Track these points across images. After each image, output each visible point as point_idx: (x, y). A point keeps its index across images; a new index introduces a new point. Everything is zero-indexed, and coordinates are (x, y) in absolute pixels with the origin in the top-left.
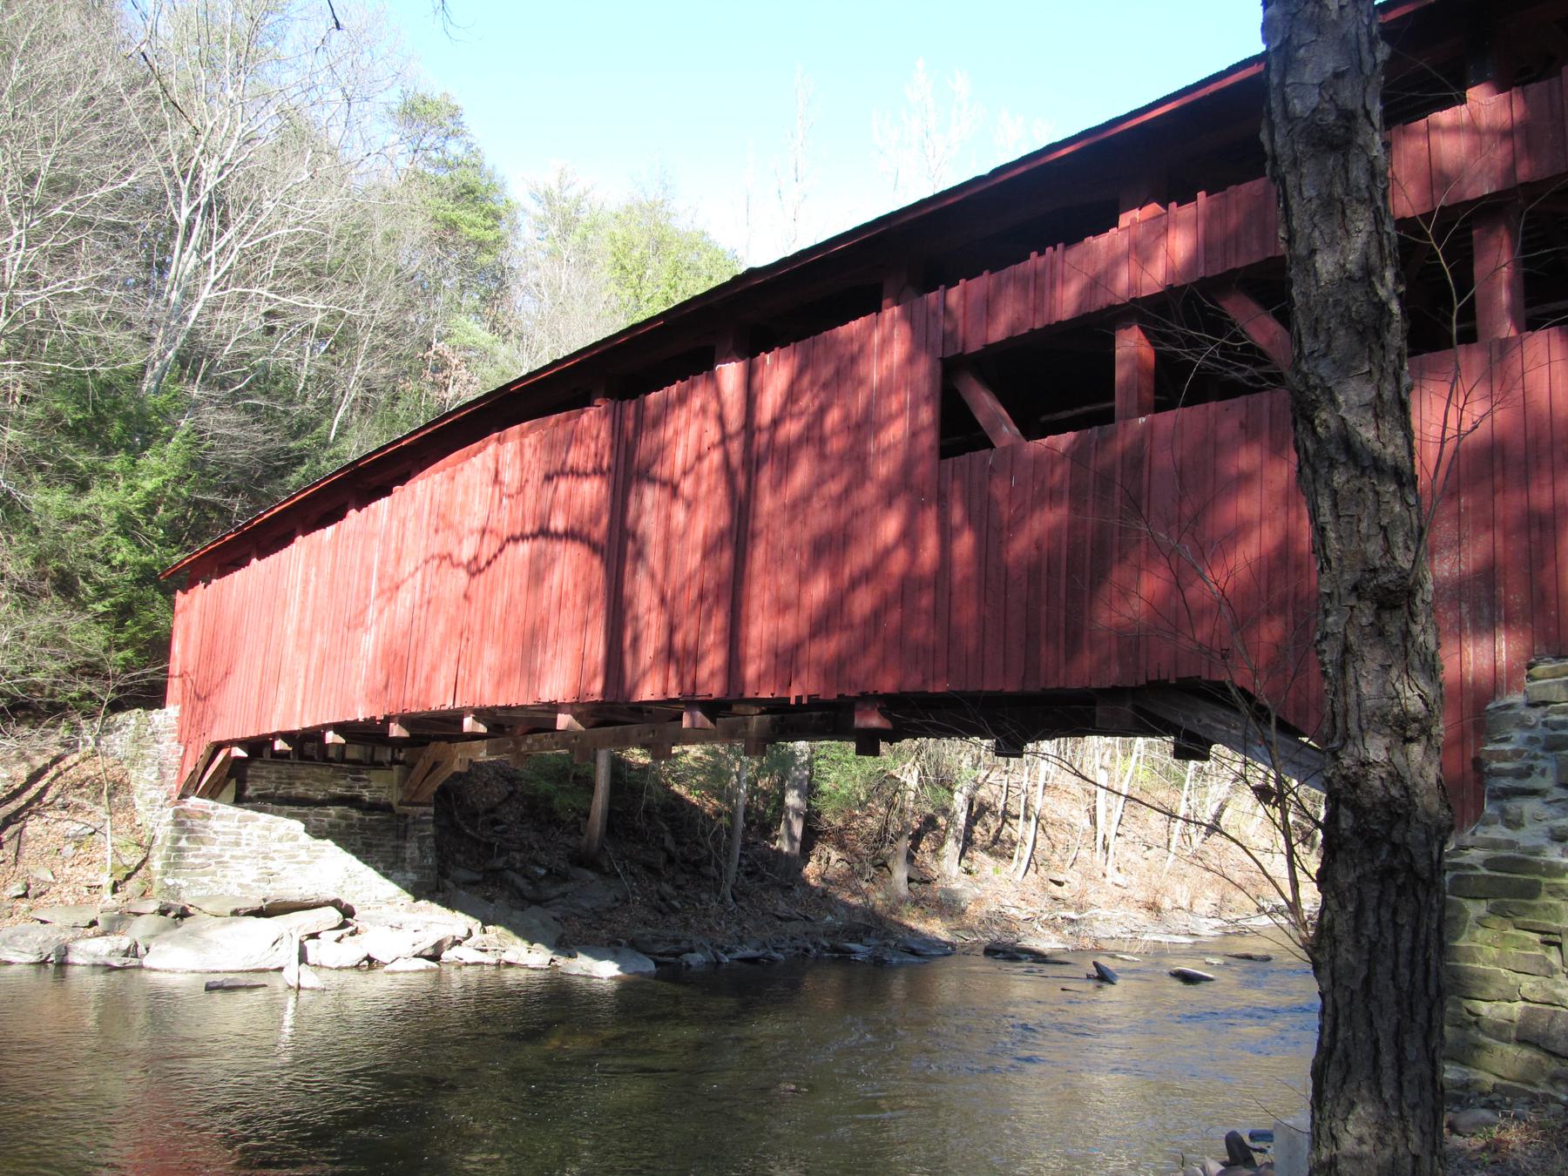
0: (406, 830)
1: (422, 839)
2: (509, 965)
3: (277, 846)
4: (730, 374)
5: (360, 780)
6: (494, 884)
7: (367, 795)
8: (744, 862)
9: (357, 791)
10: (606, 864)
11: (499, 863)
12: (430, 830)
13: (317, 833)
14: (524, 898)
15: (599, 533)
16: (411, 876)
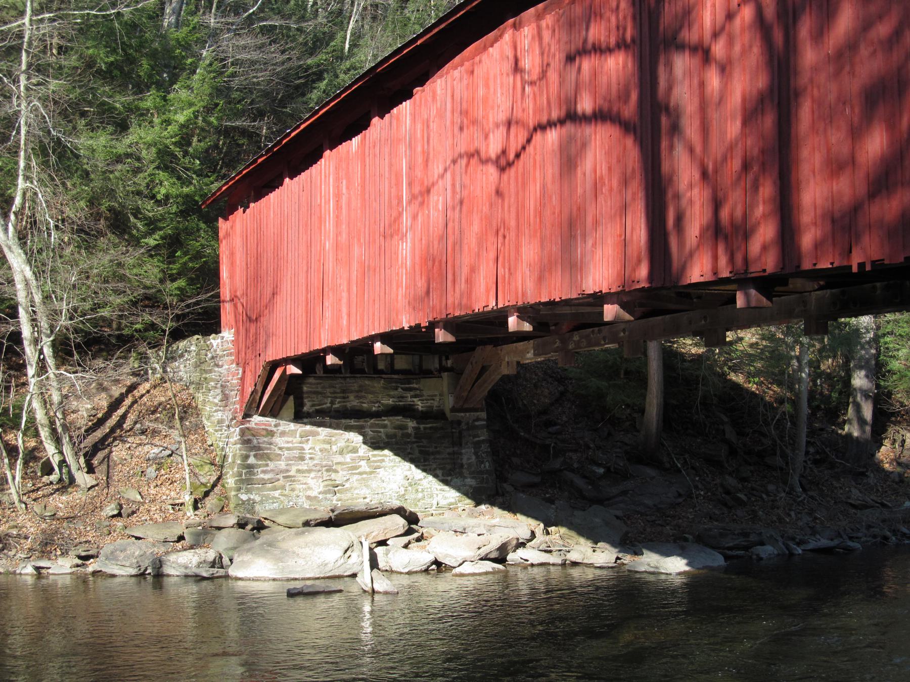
1: (477, 445)
3: (339, 458)
5: (410, 389)
7: (420, 405)
8: (812, 450)
11: (557, 464)
12: (483, 435)
13: (375, 444)
15: (629, 110)
16: (470, 481)
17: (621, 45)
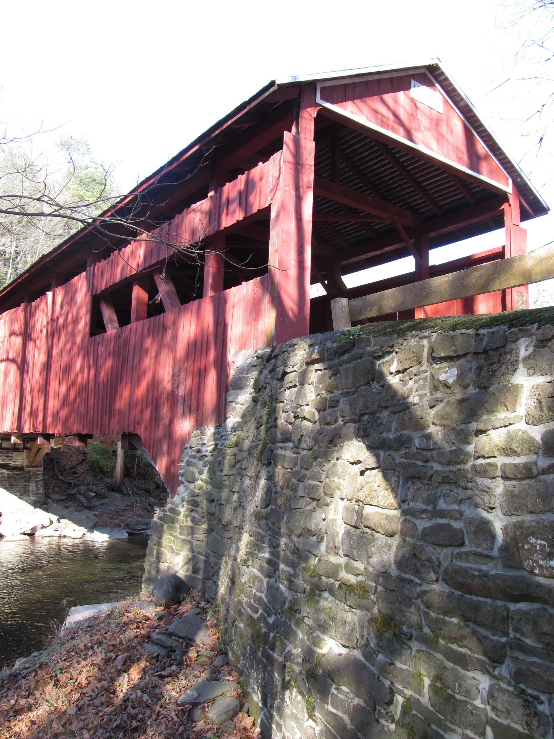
0: (30, 478)
1: (37, 482)
2: (65, 536)
4: (50, 294)
5: (8, 457)
6: (71, 501)
7: (12, 463)
9: (7, 461)
10: (124, 490)
11: (74, 491)
14: (83, 506)
16: (32, 498)
17: (21, 334)
